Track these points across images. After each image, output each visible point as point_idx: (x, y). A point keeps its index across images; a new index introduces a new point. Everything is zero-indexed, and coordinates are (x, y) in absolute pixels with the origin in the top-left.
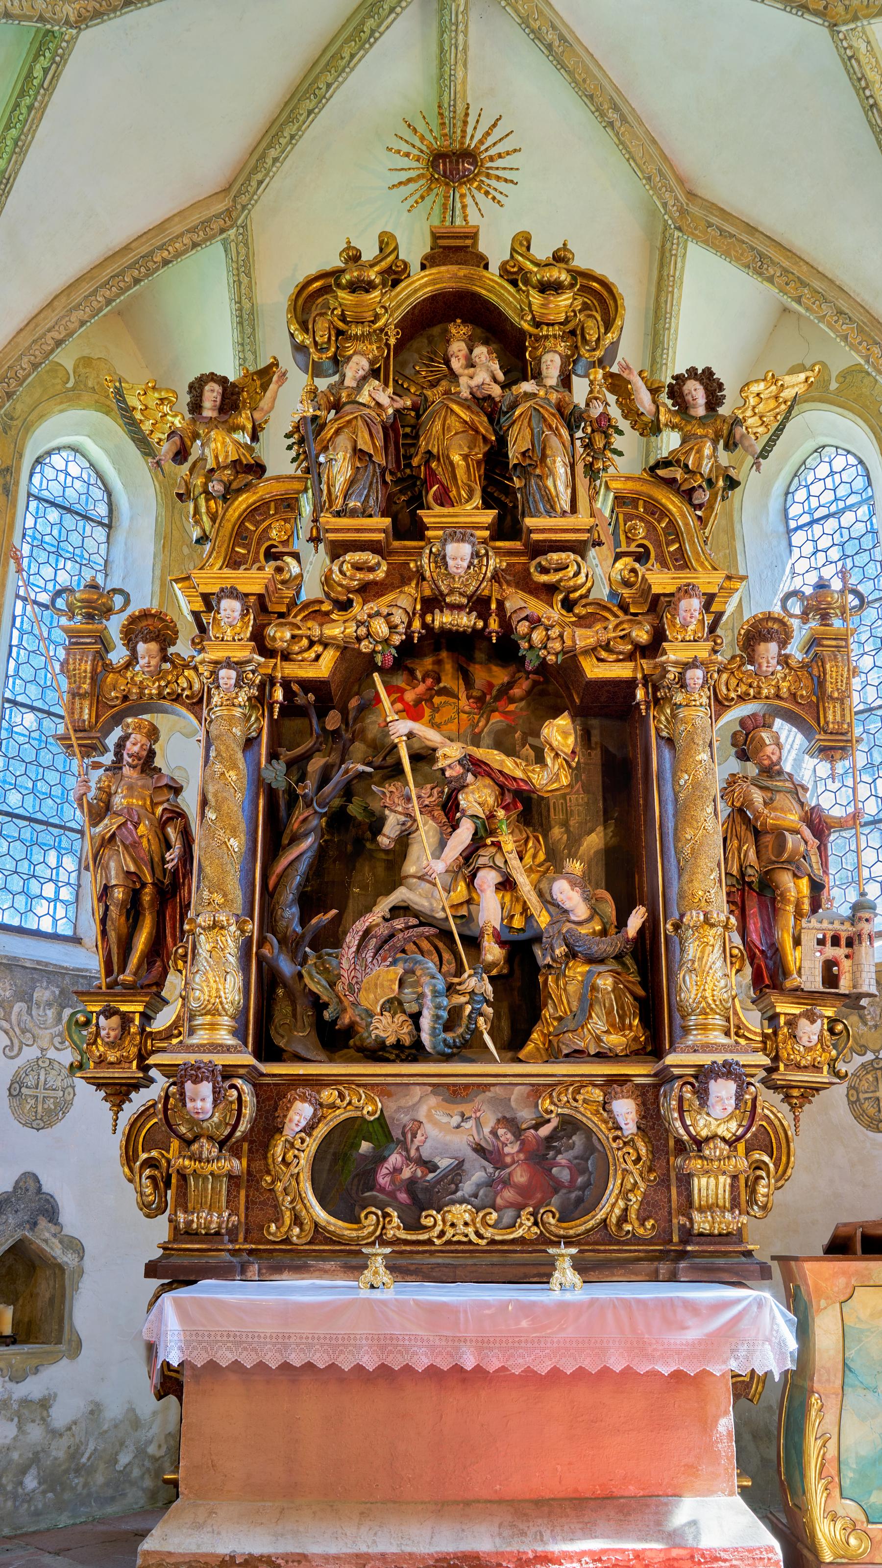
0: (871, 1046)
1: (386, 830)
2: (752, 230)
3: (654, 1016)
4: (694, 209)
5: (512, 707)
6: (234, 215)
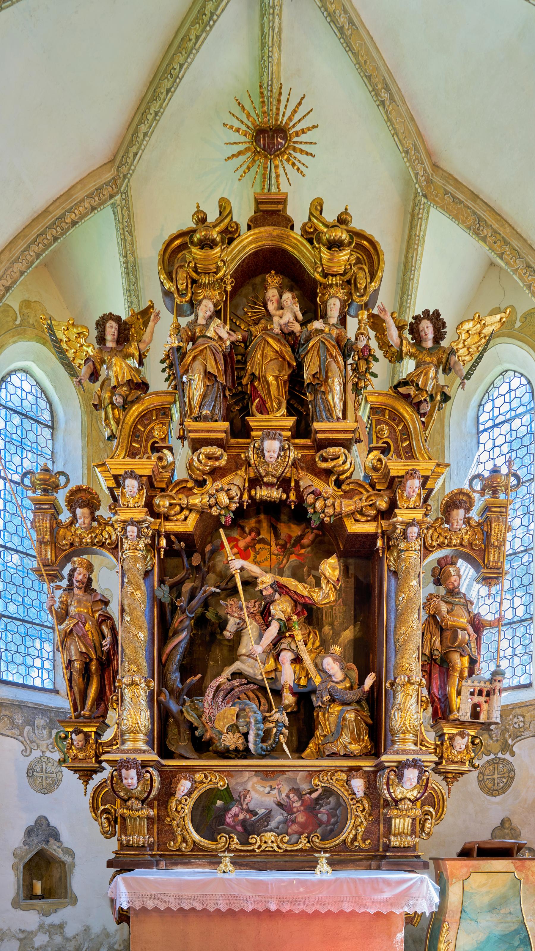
0: (493, 751)
1: (229, 627)
2: (475, 197)
3: (376, 733)
4: (437, 179)
5: (302, 551)
6: (118, 182)
